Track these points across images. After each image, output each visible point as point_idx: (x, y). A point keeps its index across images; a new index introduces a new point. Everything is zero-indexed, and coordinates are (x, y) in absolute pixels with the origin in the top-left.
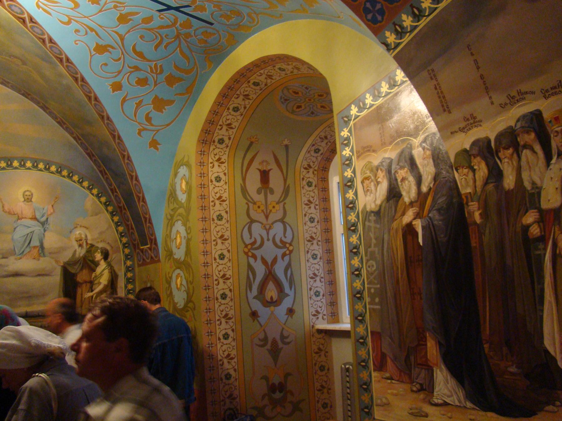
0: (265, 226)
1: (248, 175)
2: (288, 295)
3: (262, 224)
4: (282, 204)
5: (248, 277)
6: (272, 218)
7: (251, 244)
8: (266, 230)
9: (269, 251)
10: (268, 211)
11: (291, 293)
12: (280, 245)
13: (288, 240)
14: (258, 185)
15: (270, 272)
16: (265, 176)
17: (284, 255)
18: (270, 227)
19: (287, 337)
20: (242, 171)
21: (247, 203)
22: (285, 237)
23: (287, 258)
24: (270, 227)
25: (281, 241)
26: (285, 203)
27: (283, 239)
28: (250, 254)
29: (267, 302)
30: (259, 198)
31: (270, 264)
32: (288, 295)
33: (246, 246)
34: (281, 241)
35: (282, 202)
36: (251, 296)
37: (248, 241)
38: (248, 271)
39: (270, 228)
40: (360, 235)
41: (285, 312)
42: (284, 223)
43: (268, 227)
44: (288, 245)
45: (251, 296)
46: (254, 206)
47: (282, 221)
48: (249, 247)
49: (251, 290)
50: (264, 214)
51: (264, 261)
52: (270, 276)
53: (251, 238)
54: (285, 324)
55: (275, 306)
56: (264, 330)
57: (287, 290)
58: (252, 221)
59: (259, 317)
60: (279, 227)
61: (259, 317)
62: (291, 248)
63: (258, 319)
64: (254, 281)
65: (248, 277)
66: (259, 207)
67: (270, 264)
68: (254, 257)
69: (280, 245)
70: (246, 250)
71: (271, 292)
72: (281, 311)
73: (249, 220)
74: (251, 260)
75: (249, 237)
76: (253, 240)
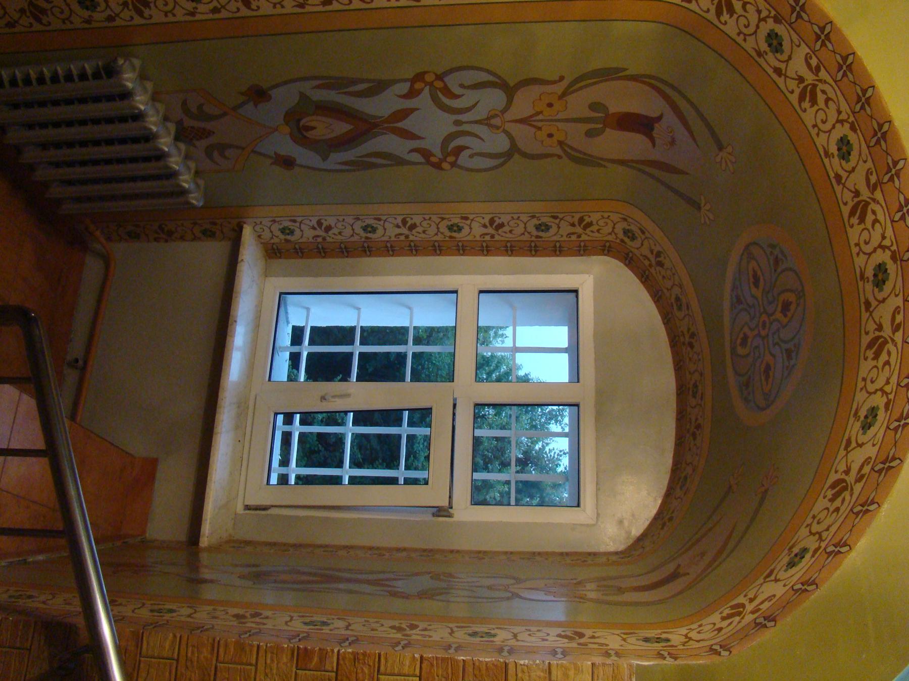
0: (497, 115)
1: (647, 88)
2: (325, 158)
3: (504, 111)
4: (557, 150)
5: (354, 82)
6: (517, 130)
7: (446, 86)
8: (488, 119)
9: (432, 125)
10: (539, 124)
11: (329, 164)
12: (453, 144)
13: (463, 159)
14: (617, 106)
15: (376, 125)
16: (641, 124)
17: (426, 154)
18: (498, 128)
19: (222, 155)
20: (665, 82)
21: (562, 78)
22: (471, 156)
23: (417, 157)
24: (498, 128)
25: (460, 149)
26: (560, 157)
27: (466, 153)
28: (418, 86)
29: (299, 121)
30: (578, 104)
31: (399, 125)
32: (325, 158)
33: (439, 77)
34: (460, 149)
35: (565, 151)
36: (307, 87)
37: (452, 82)
38: (368, 81)
39: (490, 126)
40: (457, 627)
41: (282, 153)
42: (508, 155)
43: (496, 121)
44: (451, 159)
45: (307, 87)
46: (562, 138)
47: (514, 150)
48: (438, 84)
49: (318, 87)
50: (531, 116)
51: (405, 113)
52: (366, 127)
53: (462, 86)
54: (253, 152)
55: (291, 135)
56: (225, 114)
57: (338, 157)
58: (510, 91)
59: (256, 105)
60: (501, 143)
61: (256, 105)
62: (445, 165)
63: (251, 104)
64: (345, 93)
65: (354, 82)
66: (550, 105)
67: (399, 125)
68: (412, 94)
69: (453, 144)
70: (429, 78)
71: (325, 128)
72: (286, 146)
73: (512, 84)
74: (404, 88)
75: (466, 84)
76: (457, 91)
